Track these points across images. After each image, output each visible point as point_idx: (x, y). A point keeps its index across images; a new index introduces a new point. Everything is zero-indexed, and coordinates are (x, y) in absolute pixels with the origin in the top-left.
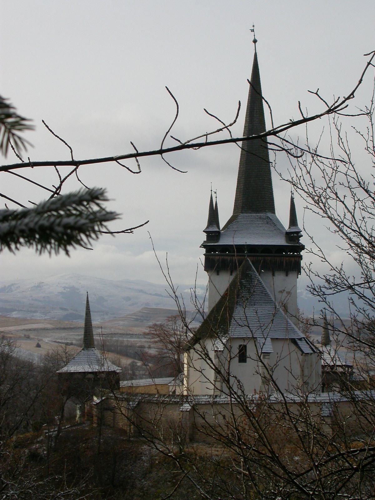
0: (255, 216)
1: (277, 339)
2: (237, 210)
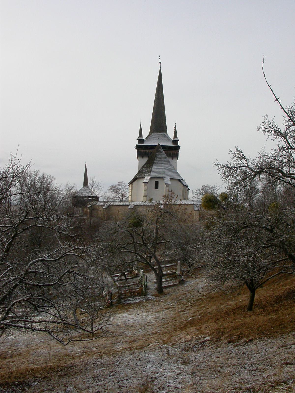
1: (172, 179)
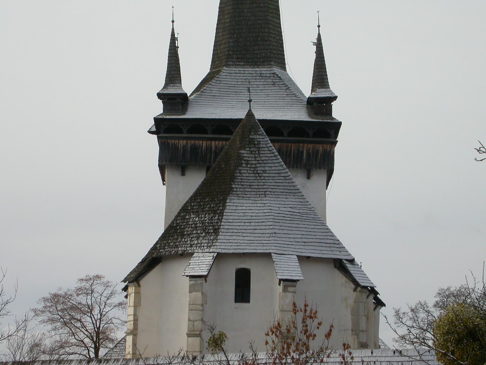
0: (252, 72)
1: (308, 258)
2: (217, 63)
